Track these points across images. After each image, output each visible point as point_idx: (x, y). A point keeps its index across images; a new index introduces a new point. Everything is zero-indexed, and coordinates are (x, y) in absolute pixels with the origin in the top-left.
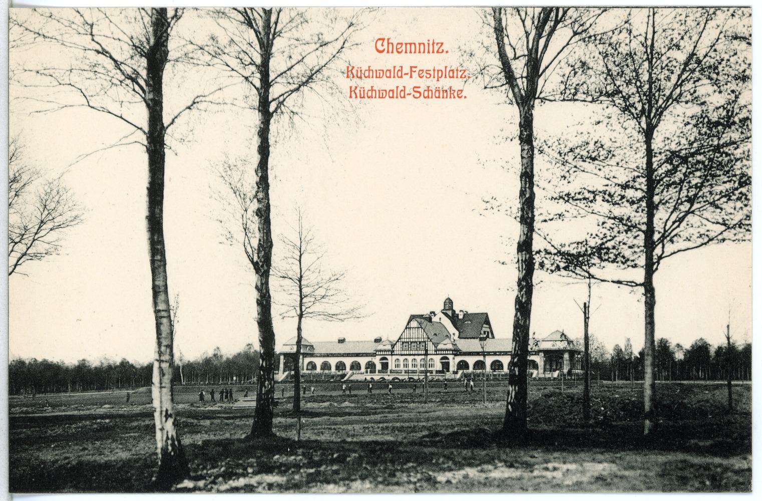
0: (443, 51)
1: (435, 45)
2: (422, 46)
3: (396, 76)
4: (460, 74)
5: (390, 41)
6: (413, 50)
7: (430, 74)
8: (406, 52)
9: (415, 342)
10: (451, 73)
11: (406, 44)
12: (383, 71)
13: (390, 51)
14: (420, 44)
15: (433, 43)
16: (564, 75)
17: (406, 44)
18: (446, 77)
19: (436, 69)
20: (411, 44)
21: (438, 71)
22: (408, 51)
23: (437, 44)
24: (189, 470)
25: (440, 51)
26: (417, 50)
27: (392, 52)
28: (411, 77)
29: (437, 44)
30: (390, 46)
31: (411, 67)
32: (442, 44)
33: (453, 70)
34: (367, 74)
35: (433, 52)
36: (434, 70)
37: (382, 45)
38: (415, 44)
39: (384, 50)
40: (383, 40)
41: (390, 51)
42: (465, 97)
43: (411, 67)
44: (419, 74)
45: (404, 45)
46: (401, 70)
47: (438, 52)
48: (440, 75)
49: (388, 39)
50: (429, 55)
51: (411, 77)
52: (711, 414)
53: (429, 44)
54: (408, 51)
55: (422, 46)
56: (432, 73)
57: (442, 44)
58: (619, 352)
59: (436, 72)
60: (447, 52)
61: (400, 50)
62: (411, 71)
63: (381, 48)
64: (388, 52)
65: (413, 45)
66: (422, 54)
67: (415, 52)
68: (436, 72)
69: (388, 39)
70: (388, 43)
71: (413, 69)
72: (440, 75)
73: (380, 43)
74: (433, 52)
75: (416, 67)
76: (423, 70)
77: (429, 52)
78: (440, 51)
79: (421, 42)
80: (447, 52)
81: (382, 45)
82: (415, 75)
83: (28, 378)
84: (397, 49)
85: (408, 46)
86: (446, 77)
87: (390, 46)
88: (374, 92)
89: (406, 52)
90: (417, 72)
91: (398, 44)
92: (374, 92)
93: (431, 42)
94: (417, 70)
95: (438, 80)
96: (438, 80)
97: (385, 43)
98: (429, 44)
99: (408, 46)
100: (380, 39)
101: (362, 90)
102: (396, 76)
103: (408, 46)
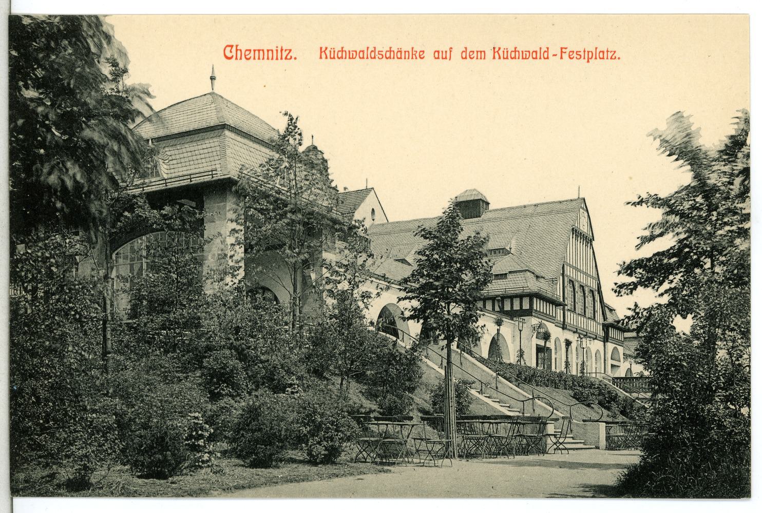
0: (615, 57)
1: (283, 51)
2: (270, 53)
4: (610, 55)
5: (238, 48)
6: (261, 57)
7: (382, 55)
8: (477, 58)
10: (601, 54)
11: (255, 51)
12: (529, 52)
13: (239, 58)
14: (268, 51)
15: (282, 50)
16: (343, 203)
17: (255, 51)
18: (596, 58)
19: (586, 50)
20: (259, 51)
22: (479, 57)
23: (286, 50)
25: (289, 57)
26: (266, 57)
27: (241, 59)
28: (561, 58)
29: (286, 50)
30: (239, 52)
31: (562, 48)
32: (290, 50)
35: (607, 58)
36: (584, 51)
37: (231, 52)
38: (263, 50)
40: (232, 46)
41: (239, 58)
42: (619, 58)
43: (562, 48)
45: (252, 52)
46: (547, 51)
47: (286, 58)
48: (590, 56)
49: (237, 46)
50: (254, 61)
53: (277, 50)
54: (479, 57)
55: (270, 53)
56: (582, 54)
59: (586, 53)
60: (295, 58)
62: (562, 52)
63: (229, 55)
64: (236, 59)
65: (261, 52)
66: (479, 60)
67: (272, 59)
68: (586, 53)
70: (237, 50)
72: (590, 56)
73: (228, 49)
74: (607, 58)
75: (566, 48)
77: (277, 59)
78: (289, 57)
80: (295, 58)
81: (231, 52)
82: (565, 56)
83: (22, 31)
84: (245, 56)
85: (479, 53)
86: (596, 58)
87: (239, 52)
88: (517, 53)
90: (568, 53)
91: (246, 50)
92: (517, 53)
94: (568, 51)
95: (588, 62)
96: (588, 62)
97: (234, 50)
98: (277, 50)
99: (257, 52)
100: (228, 46)
101: (505, 50)
102: (395, 57)
103: (257, 52)
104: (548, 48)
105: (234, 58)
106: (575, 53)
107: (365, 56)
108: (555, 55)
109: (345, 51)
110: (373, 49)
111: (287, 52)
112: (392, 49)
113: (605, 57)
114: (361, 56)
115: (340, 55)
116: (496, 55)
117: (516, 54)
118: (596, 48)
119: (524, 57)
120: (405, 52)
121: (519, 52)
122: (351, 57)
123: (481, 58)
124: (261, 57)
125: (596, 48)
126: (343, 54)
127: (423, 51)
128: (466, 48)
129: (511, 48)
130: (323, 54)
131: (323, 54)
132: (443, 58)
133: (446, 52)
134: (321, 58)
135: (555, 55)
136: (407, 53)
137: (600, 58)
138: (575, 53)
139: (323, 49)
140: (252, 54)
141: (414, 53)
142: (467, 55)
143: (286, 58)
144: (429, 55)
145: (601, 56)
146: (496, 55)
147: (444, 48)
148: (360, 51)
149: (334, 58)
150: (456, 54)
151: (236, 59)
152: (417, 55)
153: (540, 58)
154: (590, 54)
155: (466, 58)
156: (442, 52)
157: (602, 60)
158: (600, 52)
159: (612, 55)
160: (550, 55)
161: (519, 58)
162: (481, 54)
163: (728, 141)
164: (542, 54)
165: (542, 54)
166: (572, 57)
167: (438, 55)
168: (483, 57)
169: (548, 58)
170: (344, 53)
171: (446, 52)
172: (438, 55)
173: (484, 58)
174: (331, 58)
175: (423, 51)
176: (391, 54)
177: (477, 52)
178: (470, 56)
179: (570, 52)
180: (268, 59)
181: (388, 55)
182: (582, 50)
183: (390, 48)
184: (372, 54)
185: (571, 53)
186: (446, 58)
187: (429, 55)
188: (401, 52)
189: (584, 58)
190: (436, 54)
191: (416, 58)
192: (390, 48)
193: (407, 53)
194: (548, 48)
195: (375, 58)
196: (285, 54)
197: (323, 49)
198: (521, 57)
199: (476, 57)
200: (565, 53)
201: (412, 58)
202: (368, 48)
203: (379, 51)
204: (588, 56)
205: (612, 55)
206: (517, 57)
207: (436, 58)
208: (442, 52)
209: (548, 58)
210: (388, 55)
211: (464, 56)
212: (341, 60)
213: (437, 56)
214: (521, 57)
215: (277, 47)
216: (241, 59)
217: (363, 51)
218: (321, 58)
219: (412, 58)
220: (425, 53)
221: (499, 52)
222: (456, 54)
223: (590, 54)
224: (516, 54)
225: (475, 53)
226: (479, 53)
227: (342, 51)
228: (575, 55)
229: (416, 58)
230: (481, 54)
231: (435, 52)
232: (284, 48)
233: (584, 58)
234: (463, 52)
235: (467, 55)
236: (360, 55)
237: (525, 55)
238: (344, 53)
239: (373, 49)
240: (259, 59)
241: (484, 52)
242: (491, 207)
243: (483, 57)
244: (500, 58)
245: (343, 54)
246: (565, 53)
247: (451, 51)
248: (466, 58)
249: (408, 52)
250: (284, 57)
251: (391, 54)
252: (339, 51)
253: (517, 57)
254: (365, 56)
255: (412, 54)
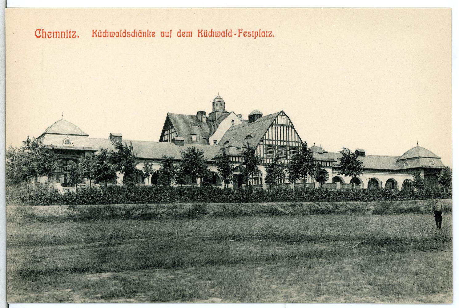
0: (76, 36)
1: (268, 33)
3: (228, 36)
5: (44, 31)
6: (58, 36)
7: (251, 34)
9: (283, 147)
10: (263, 33)
12: (220, 32)
13: (44, 37)
15: (70, 32)
17: (54, 32)
18: (260, 36)
19: (254, 31)
20: (56, 32)
21: (255, 32)
23: (72, 32)
24: (243, 182)
25: (74, 36)
26: (60, 36)
28: (239, 36)
29: (72, 32)
30: (44, 33)
32: (271, 32)
33: (264, 32)
34: (210, 34)
35: (70, 37)
36: (253, 32)
37: (39, 33)
38: (59, 32)
39: (41, 36)
40: (40, 30)
41: (44, 37)
43: (239, 30)
44: (244, 35)
45: (52, 33)
46: (231, 32)
47: (73, 37)
48: (256, 35)
49: (43, 30)
50: (121, 38)
51: (239, 36)
52: (113, 177)
53: (67, 32)
54: (188, 35)
55: (63, 33)
56: (251, 33)
57: (75, 32)
58: (172, 157)
59: (254, 33)
61: (50, 36)
62: (239, 32)
63: (38, 35)
64: (43, 37)
65: (58, 33)
68: (254, 33)
69: (43, 30)
70: (43, 32)
71: (240, 31)
72: (256, 35)
73: (38, 32)
74: (70, 37)
75: (242, 30)
76: (246, 32)
77: (67, 37)
78: (74, 36)
79: (63, 31)
80: (78, 37)
81: (39, 33)
82: (242, 35)
84: (48, 35)
85: (55, 34)
86: (260, 36)
87: (44, 33)
89: (54, 37)
91: (49, 32)
93: (68, 32)
94: (243, 32)
95: (255, 38)
96: (255, 38)
98: (67, 32)
99: (188, 33)
101: (100, 32)
102: (228, 36)
104: (231, 30)
105: (41, 37)
106: (247, 33)
107: (120, 35)
108: (236, 34)
109: (213, 32)
110: (124, 31)
111: (73, 33)
112: (136, 31)
113: (266, 35)
114: (223, 35)
115: (104, 35)
116: (94, 34)
117: (212, 34)
118: (260, 30)
119: (217, 35)
120: (144, 32)
121: (108, 32)
122: (217, 35)
123: (189, 36)
124: (58, 36)
125: (260, 30)
126: (107, 34)
127: (154, 32)
128: (180, 30)
129: (103, 31)
130: (200, 34)
131: (200, 34)
132: (166, 36)
133: (168, 32)
134: (199, 36)
135: (236, 34)
136: (145, 33)
137: (123, 36)
138: (247, 33)
139: (200, 31)
140: (52, 35)
141: (149, 33)
142: (181, 34)
143: (73, 37)
144: (158, 34)
145: (140, 35)
146: (94, 34)
147: (167, 30)
148: (116, 33)
149: (101, 36)
150: (174, 34)
151: (43, 37)
152: (151, 34)
153: (227, 36)
154: (256, 33)
155: (180, 36)
156: (166, 32)
157: (263, 37)
158: (262, 32)
159: (270, 34)
160: (232, 35)
161: (214, 36)
162: (190, 34)
163: (170, 157)
164: (226, 34)
165: (226, 34)
166: (245, 35)
167: (163, 34)
168: (190, 36)
169: (231, 36)
170: (213, 33)
171: (168, 32)
172: (163, 34)
173: (191, 36)
174: (99, 36)
175: (154, 32)
176: (136, 34)
177: (187, 32)
178: (182, 35)
179: (244, 32)
180: (62, 37)
181: (133, 34)
182: (252, 31)
183: (212, 30)
184: (124, 34)
185: (245, 33)
186: (168, 36)
187: (158, 34)
188: (141, 32)
189: (253, 36)
190: (162, 34)
191: (150, 36)
192: (212, 30)
193: (145, 33)
194: (231, 30)
195: (125, 36)
196: (72, 35)
197: (95, 31)
198: (109, 36)
199: (186, 36)
200: (241, 33)
201: (148, 36)
202: (121, 30)
203: (128, 32)
204: (256, 34)
205: (270, 34)
206: (107, 35)
207: (162, 36)
208: (166, 32)
209: (231, 36)
210: (133, 34)
211: (179, 35)
212: (211, 37)
213: (162, 35)
214: (109, 36)
215: (67, 30)
216: (45, 37)
217: (224, 32)
218: (199, 36)
219: (148, 36)
220: (156, 33)
221: (96, 33)
222: (174, 34)
223: (256, 33)
224: (212, 34)
225: (186, 33)
226: (55, 34)
227: (135, 32)
228: (247, 34)
229: (150, 36)
230: (190, 34)
231: (162, 32)
232: (71, 31)
233: (253, 36)
234: (179, 32)
235: (181, 34)
236: (117, 34)
237: (218, 34)
238: (213, 33)
239: (179, 31)
240: (56, 37)
241: (191, 32)
242: (263, 116)
243: (190, 36)
244: (96, 36)
245: (107, 34)
246: (241, 33)
247: (171, 32)
248: (180, 36)
249: (257, 32)
250: (71, 36)
251: (136, 34)
252: (104, 32)
253: (107, 35)
254: (120, 35)
255: (148, 34)
